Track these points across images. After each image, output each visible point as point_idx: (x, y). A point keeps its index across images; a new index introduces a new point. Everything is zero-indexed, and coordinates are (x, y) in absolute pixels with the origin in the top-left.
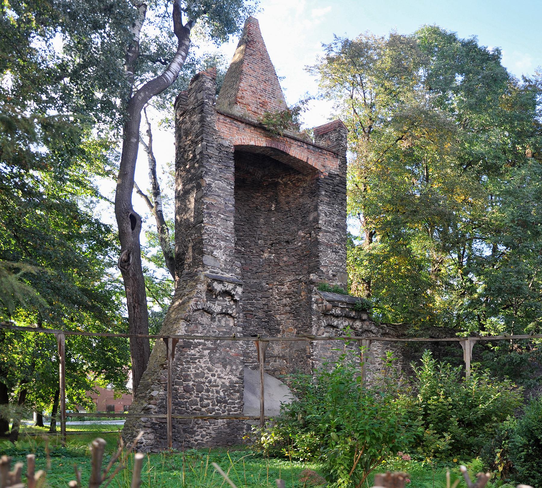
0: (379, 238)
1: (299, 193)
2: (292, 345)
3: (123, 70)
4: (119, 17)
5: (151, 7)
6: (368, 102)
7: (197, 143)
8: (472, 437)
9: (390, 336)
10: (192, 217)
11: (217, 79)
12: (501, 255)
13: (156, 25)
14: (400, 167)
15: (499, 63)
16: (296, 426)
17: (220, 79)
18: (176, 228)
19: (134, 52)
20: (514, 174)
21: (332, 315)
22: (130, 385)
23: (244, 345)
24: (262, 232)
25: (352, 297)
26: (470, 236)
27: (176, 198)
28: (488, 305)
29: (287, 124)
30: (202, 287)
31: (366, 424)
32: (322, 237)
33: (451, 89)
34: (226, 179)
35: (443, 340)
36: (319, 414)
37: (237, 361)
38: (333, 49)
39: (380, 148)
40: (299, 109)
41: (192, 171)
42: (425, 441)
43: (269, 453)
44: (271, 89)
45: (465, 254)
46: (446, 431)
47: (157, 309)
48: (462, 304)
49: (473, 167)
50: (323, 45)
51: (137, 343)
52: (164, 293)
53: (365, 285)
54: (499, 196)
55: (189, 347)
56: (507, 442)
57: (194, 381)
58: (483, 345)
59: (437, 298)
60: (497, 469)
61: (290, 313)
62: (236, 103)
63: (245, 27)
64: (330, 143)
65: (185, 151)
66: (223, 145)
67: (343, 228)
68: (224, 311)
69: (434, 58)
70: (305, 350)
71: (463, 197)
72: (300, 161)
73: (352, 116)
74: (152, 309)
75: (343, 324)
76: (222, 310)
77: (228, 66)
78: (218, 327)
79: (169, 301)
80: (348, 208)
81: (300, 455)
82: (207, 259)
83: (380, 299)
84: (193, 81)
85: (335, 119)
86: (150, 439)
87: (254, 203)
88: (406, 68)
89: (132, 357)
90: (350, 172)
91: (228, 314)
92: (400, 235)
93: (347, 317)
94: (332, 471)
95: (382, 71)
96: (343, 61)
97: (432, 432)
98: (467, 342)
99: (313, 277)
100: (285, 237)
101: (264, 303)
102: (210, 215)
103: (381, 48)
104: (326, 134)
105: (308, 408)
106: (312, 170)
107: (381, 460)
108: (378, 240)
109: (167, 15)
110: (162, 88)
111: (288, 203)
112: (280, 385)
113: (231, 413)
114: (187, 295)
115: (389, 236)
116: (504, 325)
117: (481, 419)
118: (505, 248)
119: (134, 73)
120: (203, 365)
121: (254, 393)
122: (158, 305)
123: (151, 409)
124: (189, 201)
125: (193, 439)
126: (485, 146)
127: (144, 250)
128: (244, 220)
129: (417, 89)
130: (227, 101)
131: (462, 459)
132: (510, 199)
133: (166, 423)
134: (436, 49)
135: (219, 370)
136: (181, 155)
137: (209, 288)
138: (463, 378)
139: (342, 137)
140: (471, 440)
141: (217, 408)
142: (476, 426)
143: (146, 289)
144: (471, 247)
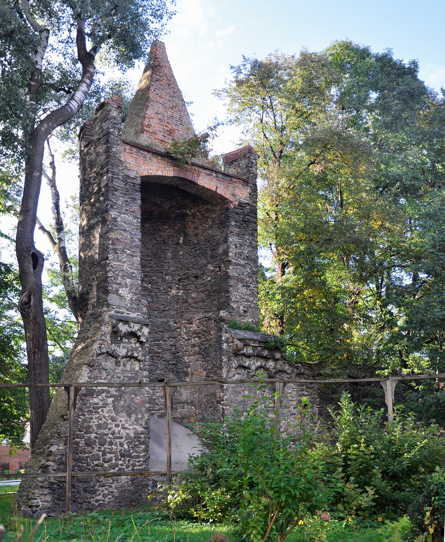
0: (291, 269)
1: (208, 224)
2: (201, 389)
3: (25, 101)
4: (20, 44)
5: (54, 32)
6: (279, 125)
7: (102, 175)
8: (398, 492)
9: (306, 376)
10: (96, 253)
11: (123, 106)
12: (423, 283)
13: (59, 51)
14: (313, 193)
15: (416, 76)
16: (205, 481)
17: (126, 106)
18: (80, 266)
19: (36, 81)
20: (434, 195)
21: (244, 355)
22: (27, 439)
23: (150, 391)
24: (169, 267)
25: (265, 334)
26: (388, 264)
27: (80, 233)
28: (410, 339)
29: (196, 152)
30: (106, 329)
31: (281, 480)
32: (232, 271)
33: (365, 107)
35: (362, 380)
36: (231, 468)
37: (143, 409)
38: (242, 71)
39: (292, 174)
40: (207, 135)
41: (98, 205)
42: (346, 497)
43: (176, 513)
44: (178, 116)
45: (384, 283)
46: (369, 485)
47: (58, 353)
48: (382, 339)
49: (390, 190)
50: (232, 67)
51: (36, 392)
52: (66, 335)
53: (278, 321)
54: (418, 219)
56: (437, 498)
57: (96, 433)
58: (406, 385)
59: (355, 333)
60: (427, 530)
62: (143, 132)
63: (151, 52)
64: (239, 171)
65: (90, 184)
67: (255, 260)
68: (129, 354)
69: (347, 76)
70: (214, 395)
71: (380, 223)
72: (208, 190)
73: (261, 140)
74: (53, 353)
75: (255, 363)
76: (127, 353)
77: (134, 93)
78: (123, 371)
79: (71, 344)
80: (259, 238)
81: (209, 515)
82: (112, 299)
83: (294, 336)
84: (98, 110)
85: (244, 145)
86: (47, 502)
87: (161, 236)
88: (318, 88)
89: (31, 409)
90: (261, 200)
91: (134, 357)
92: (313, 266)
93: (259, 356)
94: (244, 536)
95: (292, 92)
96: (252, 83)
97: (353, 486)
98: (388, 383)
99: (223, 313)
100: (194, 272)
101: (171, 343)
102: (115, 250)
103: (291, 68)
104: (236, 161)
105: (219, 461)
106: (221, 199)
107: (298, 521)
108: (291, 272)
109: (70, 41)
110: (66, 118)
111: (196, 235)
112: (189, 435)
113: (135, 468)
114: (91, 338)
115: (302, 267)
116: (428, 361)
117: (407, 470)
118: (426, 275)
119: (37, 103)
120: (107, 415)
121: (160, 444)
122: (60, 349)
123: (49, 466)
124: (94, 237)
125: (94, 500)
126: (402, 167)
127: (45, 290)
128: (151, 254)
129: (329, 109)
130: (133, 130)
131: (387, 518)
132: (430, 222)
133: (65, 482)
134: (349, 66)
135: (123, 419)
136: (85, 189)
137: (114, 330)
138: (385, 423)
139: (252, 163)
140: (397, 495)
141: (120, 462)
142: (402, 479)
143: (48, 332)
144: (390, 276)
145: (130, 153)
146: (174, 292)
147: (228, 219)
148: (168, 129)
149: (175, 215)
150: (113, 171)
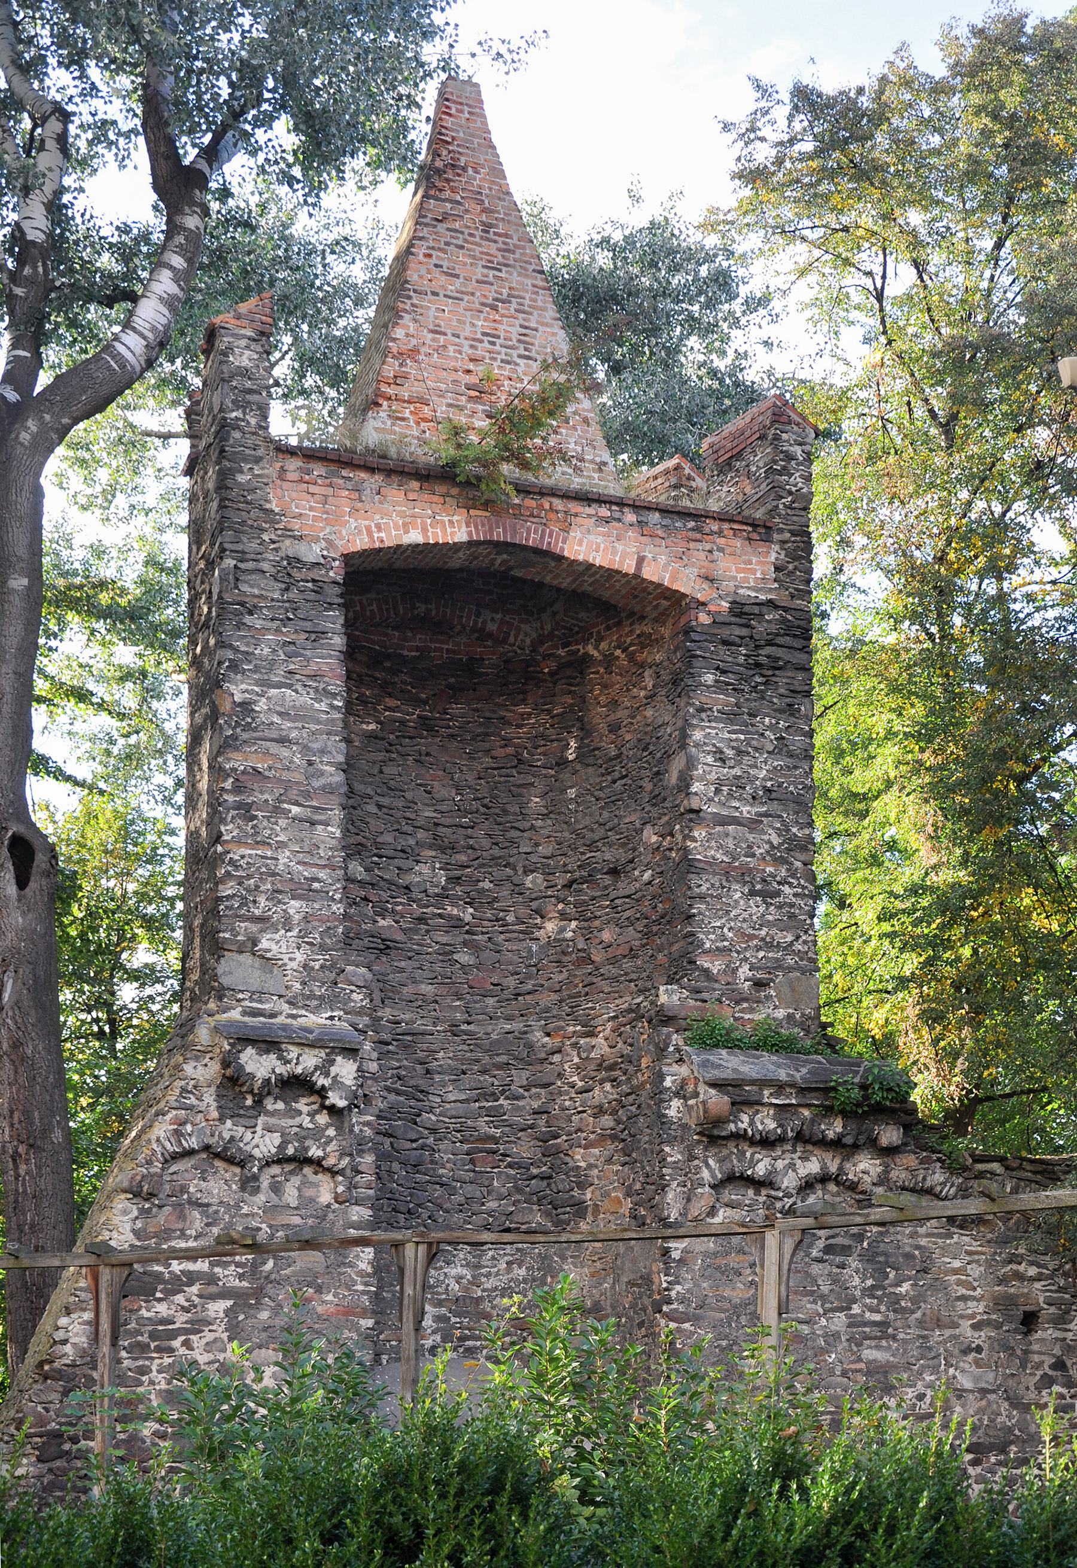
21: (739, 1136)
24: (537, 845)
34: (312, 677)
37: (347, 1334)
44: (515, 331)
55: (148, 1292)
61: (614, 1138)
64: (748, 490)
66: (299, 561)
68: (290, 1151)
70: (647, 1280)
72: (611, 574)
76: (282, 1147)
78: (270, 1210)
87: (507, 742)
91: (309, 1161)
93: (806, 1139)
101: (535, 1104)
102: (246, 811)
104: (738, 456)
106: (665, 598)
110: (105, 391)
111: (614, 728)
137: (229, 1072)
139: (789, 457)
145: (301, 481)
146: (551, 926)
147: (690, 665)
148: (473, 379)
149: (554, 665)
150: (239, 547)
